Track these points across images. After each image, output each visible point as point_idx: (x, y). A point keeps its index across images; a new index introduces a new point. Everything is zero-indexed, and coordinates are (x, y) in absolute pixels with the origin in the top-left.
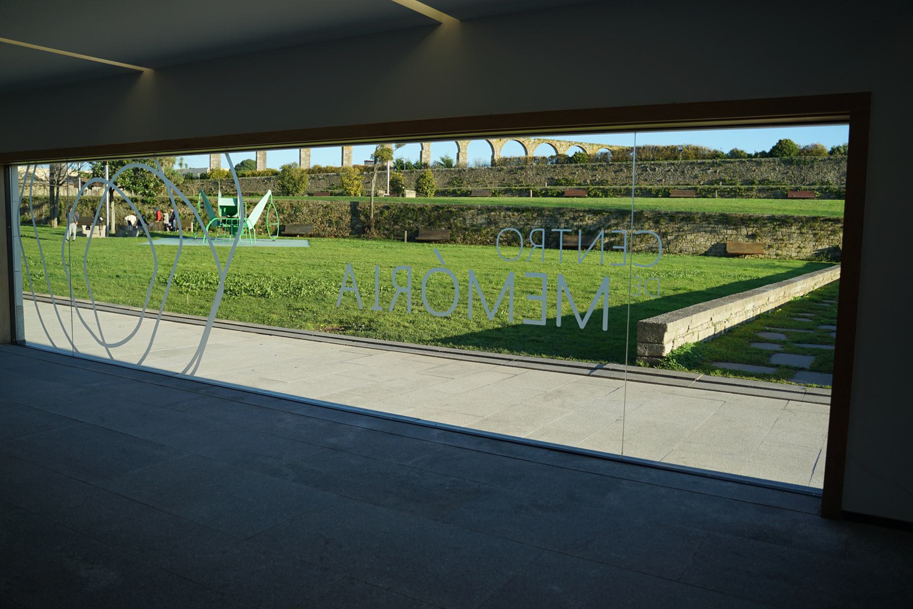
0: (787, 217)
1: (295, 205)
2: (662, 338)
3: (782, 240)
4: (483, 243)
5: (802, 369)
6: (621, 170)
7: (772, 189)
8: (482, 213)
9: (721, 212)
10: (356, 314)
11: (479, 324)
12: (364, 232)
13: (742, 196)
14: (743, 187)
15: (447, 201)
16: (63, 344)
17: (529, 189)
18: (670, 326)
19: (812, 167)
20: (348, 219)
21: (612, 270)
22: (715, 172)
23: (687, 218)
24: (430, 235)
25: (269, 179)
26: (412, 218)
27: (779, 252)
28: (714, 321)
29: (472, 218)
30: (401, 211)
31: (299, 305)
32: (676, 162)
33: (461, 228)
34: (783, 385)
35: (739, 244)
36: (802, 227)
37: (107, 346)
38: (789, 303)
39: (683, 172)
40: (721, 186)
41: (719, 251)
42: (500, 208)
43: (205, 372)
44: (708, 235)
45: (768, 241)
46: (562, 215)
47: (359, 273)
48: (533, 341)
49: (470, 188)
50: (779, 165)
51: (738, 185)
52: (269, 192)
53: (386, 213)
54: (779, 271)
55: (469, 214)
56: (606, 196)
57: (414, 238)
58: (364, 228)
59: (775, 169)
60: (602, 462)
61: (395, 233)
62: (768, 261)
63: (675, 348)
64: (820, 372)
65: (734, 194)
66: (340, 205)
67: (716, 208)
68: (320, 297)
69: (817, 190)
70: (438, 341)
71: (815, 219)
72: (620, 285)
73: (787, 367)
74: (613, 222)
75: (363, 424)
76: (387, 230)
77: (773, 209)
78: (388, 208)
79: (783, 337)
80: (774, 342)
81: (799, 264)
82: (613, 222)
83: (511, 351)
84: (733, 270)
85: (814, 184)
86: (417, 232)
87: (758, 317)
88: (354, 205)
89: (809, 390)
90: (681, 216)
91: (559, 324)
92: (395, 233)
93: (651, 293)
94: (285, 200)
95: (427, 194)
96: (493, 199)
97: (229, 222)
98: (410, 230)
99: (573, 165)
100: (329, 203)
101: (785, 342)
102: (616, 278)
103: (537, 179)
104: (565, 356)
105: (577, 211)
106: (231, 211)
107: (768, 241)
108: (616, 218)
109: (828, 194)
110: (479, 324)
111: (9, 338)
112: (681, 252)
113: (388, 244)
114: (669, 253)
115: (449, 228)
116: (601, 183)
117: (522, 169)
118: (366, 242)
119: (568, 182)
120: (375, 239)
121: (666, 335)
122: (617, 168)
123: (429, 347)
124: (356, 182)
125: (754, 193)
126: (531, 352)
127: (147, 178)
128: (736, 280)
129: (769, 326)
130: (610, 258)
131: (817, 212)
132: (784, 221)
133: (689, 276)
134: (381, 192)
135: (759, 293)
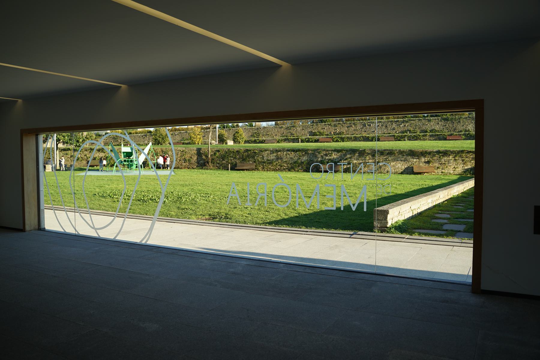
0: (446, 151)
1: (164, 150)
2: (386, 218)
3: (445, 164)
4: (275, 170)
5: (460, 231)
6: (351, 126)
7: (438, 135)
8: (273, 153)
9: (409, 149)
10: (216, 210)
11: (286, 214)
12: (205, 165)
13: (420, 139)
14: (421, 134)
15: (253, 146)
16: (70, 230)
17: (298, 138)
18: (390, 211)
19: (459, 122)
20: (195, 158)
21: (351, 184)
22: (405, 126)
23: (390, 153)
24: (243, 166)
25: (146, 136)
26: (232, 157)
27: (443, 171)
28: (412, 208)
29: (268, 156)
30: (226, 153)
31: (183, 207)
32: (382, 120)
33: (261, 162)
34: (450, 239)
35: (420, 167)
36: (456, 156)
37: (96, 229)
38: (451, 198)
39: (386, 126)
40: (408, 134)
41: (409, 171)
42: (283, 150)
43: (153, 241)
44: (402, 162)
45: (437, 165)
46: (319, 153)
47: (211, 189)
48: (317, 222)
49: (264, 138)
50: (441, 121)
51: (418, 133)
52: (151, 144)
53: (218, 154)
54: (444, 182)
55: (265, 154)
56: (343, 141)
57: (234, 168)
58: (205, 163)
59: (438, 124)
60: (366, 275)
61: (223, 165)
62: (437, 176)
63: (393, 223)
64: (469, 232)
65: (416, 138)
66: (191, 150)
67: (407, 147)
68: (194, 202)
69: (463, 135)
70: (266, 223)
71: (462, 151)
72: (358, 192)
73: (452, 231)
74: (348, 156)
75: (244, 262)
76: (218, 164)
77: (438, 147)
78: (218, 151)
79: (449, 216)
80: (444, 219)
81: (455, 177)
82: (348, 156)
83: (307, 227)
84: (419, 182)
85: (461, 131)
86: (236, 164)
87: (434, 206)
88: (199, 150)
89: (463, 241)
90: (387, 152)
91: (342, 209)
92: (223, 165)
93: (375, 195)
94: (159, 148)
95: (240, 142)
96: (278, 144)
97: (128, 161)
98: (232, 164)
99: (324, 123)
100: (184, 149)
101: (449, 219)
102: (354, 188)
103: (303, 132)
104: (336, 229)
105: (327, 151)
106: (129, 155)
107: (437, 165)
108: (350, 154)
109: (468, 137)
110: (286, 214)
111: (37, 227)
112: (387, 172)
113: (220, 172)
114: (381, 173)
115: (254, 162)
116: (340, 133)
117: (294, 126)
118: (207, 171)
119: (321, 134)
120: (211, 169)
121: (388, 215)
122: (349, 125)
123: (261, 226)
124: (199, 136)
125: (428, 137)
126: (317, 228)
127: (78, 137)
128: (421, 187)
129: (441, 210)
130: (348, 177)
131: (464, 147)
132: (445, 153)
133: (395, 186)
134: (213, 142)
135: (434, 193)
